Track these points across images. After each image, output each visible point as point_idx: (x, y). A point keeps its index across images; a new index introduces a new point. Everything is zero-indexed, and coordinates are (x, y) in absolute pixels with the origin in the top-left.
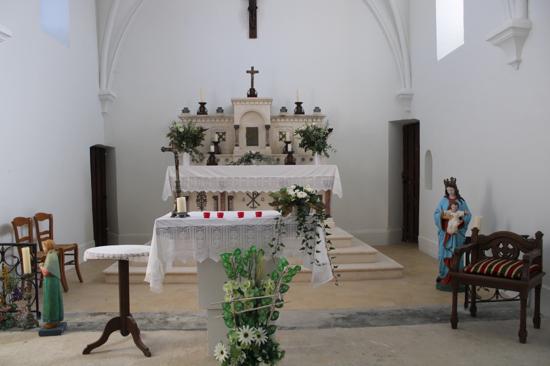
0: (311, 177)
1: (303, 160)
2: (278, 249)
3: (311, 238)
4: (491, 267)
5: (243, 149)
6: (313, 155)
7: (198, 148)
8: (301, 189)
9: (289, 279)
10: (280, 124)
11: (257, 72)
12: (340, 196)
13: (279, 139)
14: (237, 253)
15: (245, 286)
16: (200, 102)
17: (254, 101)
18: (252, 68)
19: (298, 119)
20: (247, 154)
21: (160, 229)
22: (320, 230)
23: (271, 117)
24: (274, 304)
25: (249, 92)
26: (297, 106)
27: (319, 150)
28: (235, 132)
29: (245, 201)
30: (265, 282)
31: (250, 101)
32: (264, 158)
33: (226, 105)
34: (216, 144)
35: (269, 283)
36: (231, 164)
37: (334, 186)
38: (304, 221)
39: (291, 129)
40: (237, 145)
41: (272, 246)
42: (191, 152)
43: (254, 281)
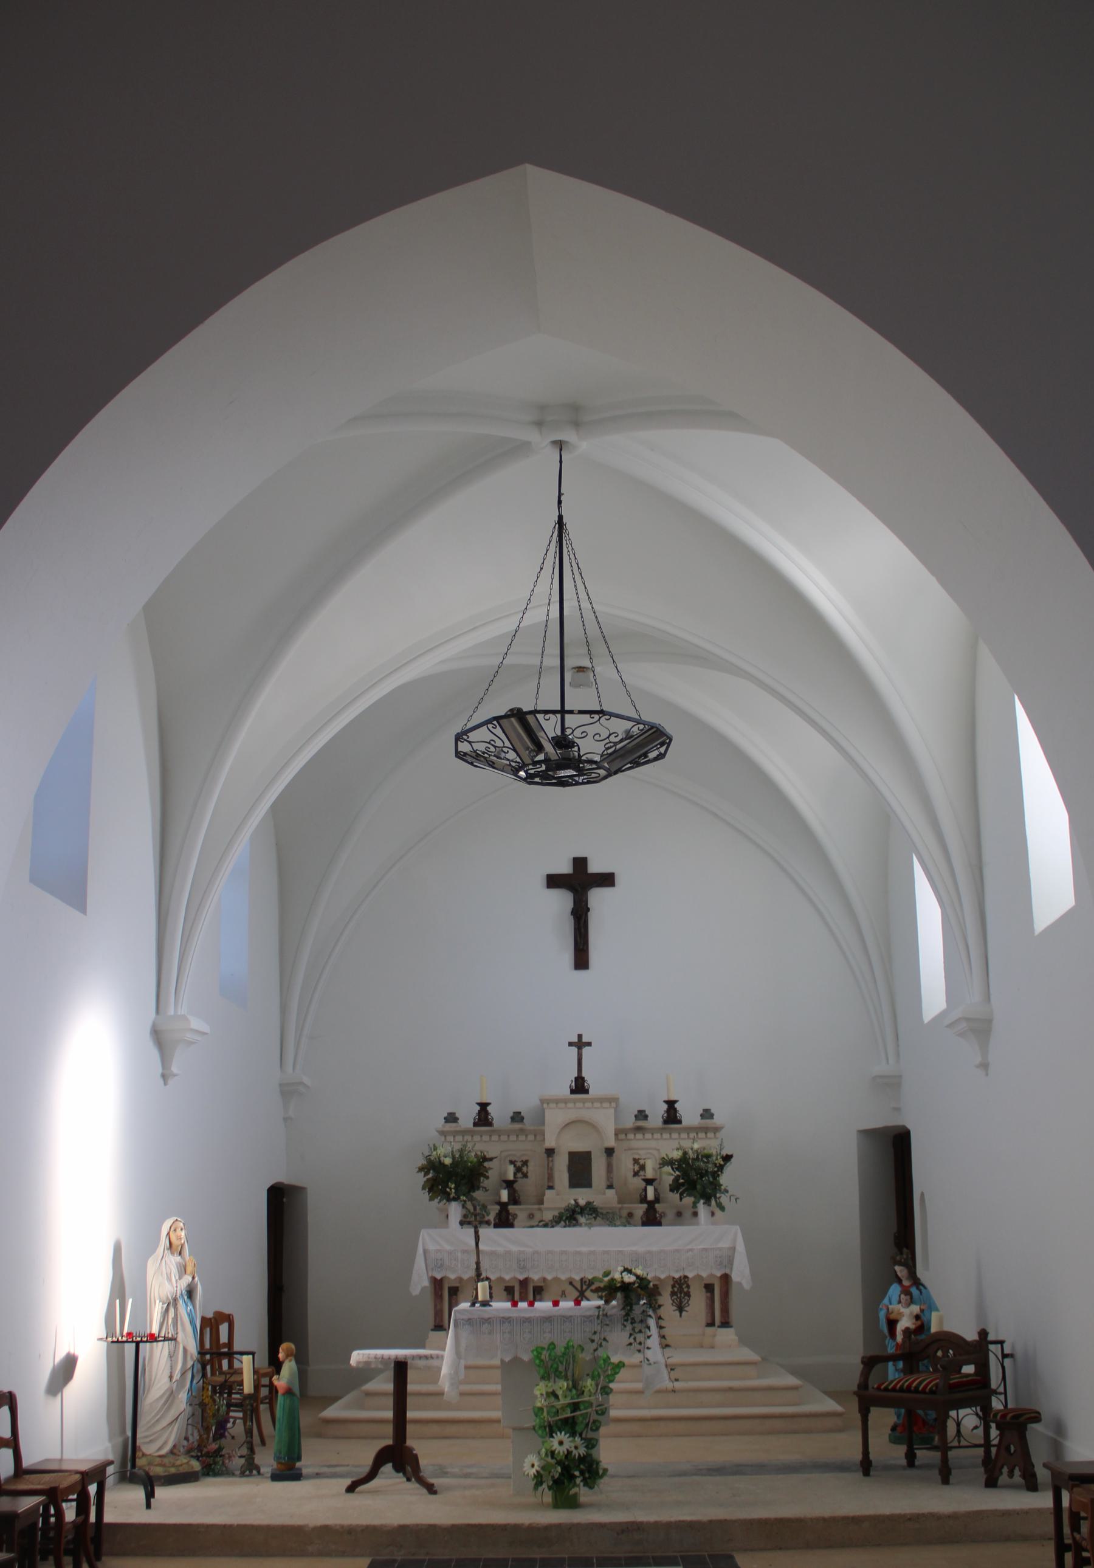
0: (691, 1250)
1: (679, 1214)
2: (601, 1345)
3: (640, 1331)
4: (920, 1383)
5: (562, 1196)
6: (695, 1205)
7: (477, 1194)
8: (630, 1271)
9: (611, 1378)
10: (635, 1144)
11: (589, 1044)
12: (747, 1285)
13: (632, 1173)
14: (551, 1347)
15: (560, 1388)
16: (479, 1102)
17: (584, 1101)
18: (580, 1036)
19: (670, 1134)
20: (570, 1206)
21: (459, 1321)
22: (652, 1322)
23: (615, 1132)
24: (594, 1409)
25: (574, 1083)
26: (669, 1106)
27: (707, 1199)
28: (546, 1163)
29: (565, 1296)
30: (584, 1384)
31: (574, 1101)
32: (602, 1214)
33: (526, 1103)
34: (509, 1185)
35: (589, 1383)
36: (541, 1224)
37: (734, 1266)
38: (631, 1310)
39: (655, 1153)
40: (551, 1188)
41: (593, 1341)
42: (465, 1201)
43: (571, 1383)
